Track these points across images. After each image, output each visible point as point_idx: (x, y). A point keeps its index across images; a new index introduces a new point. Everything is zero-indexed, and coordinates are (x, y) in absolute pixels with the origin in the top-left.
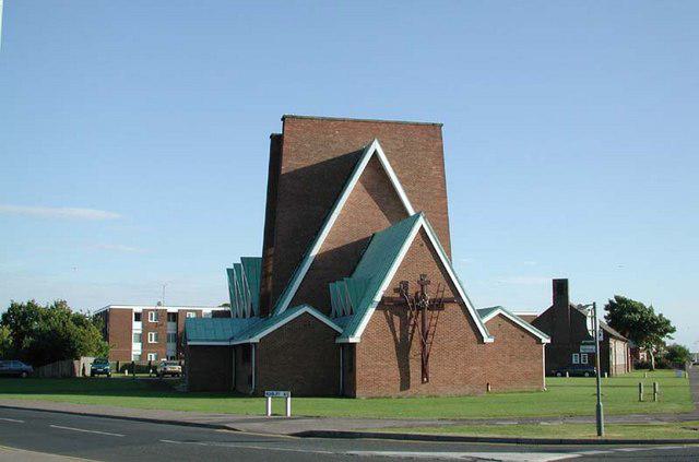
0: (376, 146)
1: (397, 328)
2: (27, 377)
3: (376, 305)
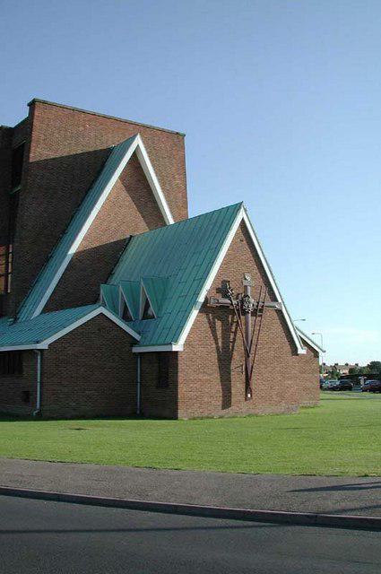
0: (138, 141)
1: (219, 333)
3: (199, 306)
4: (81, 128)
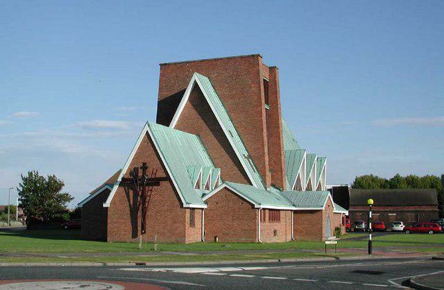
1: (131, 198)
2: (68, 228)
4: (187, 73)
